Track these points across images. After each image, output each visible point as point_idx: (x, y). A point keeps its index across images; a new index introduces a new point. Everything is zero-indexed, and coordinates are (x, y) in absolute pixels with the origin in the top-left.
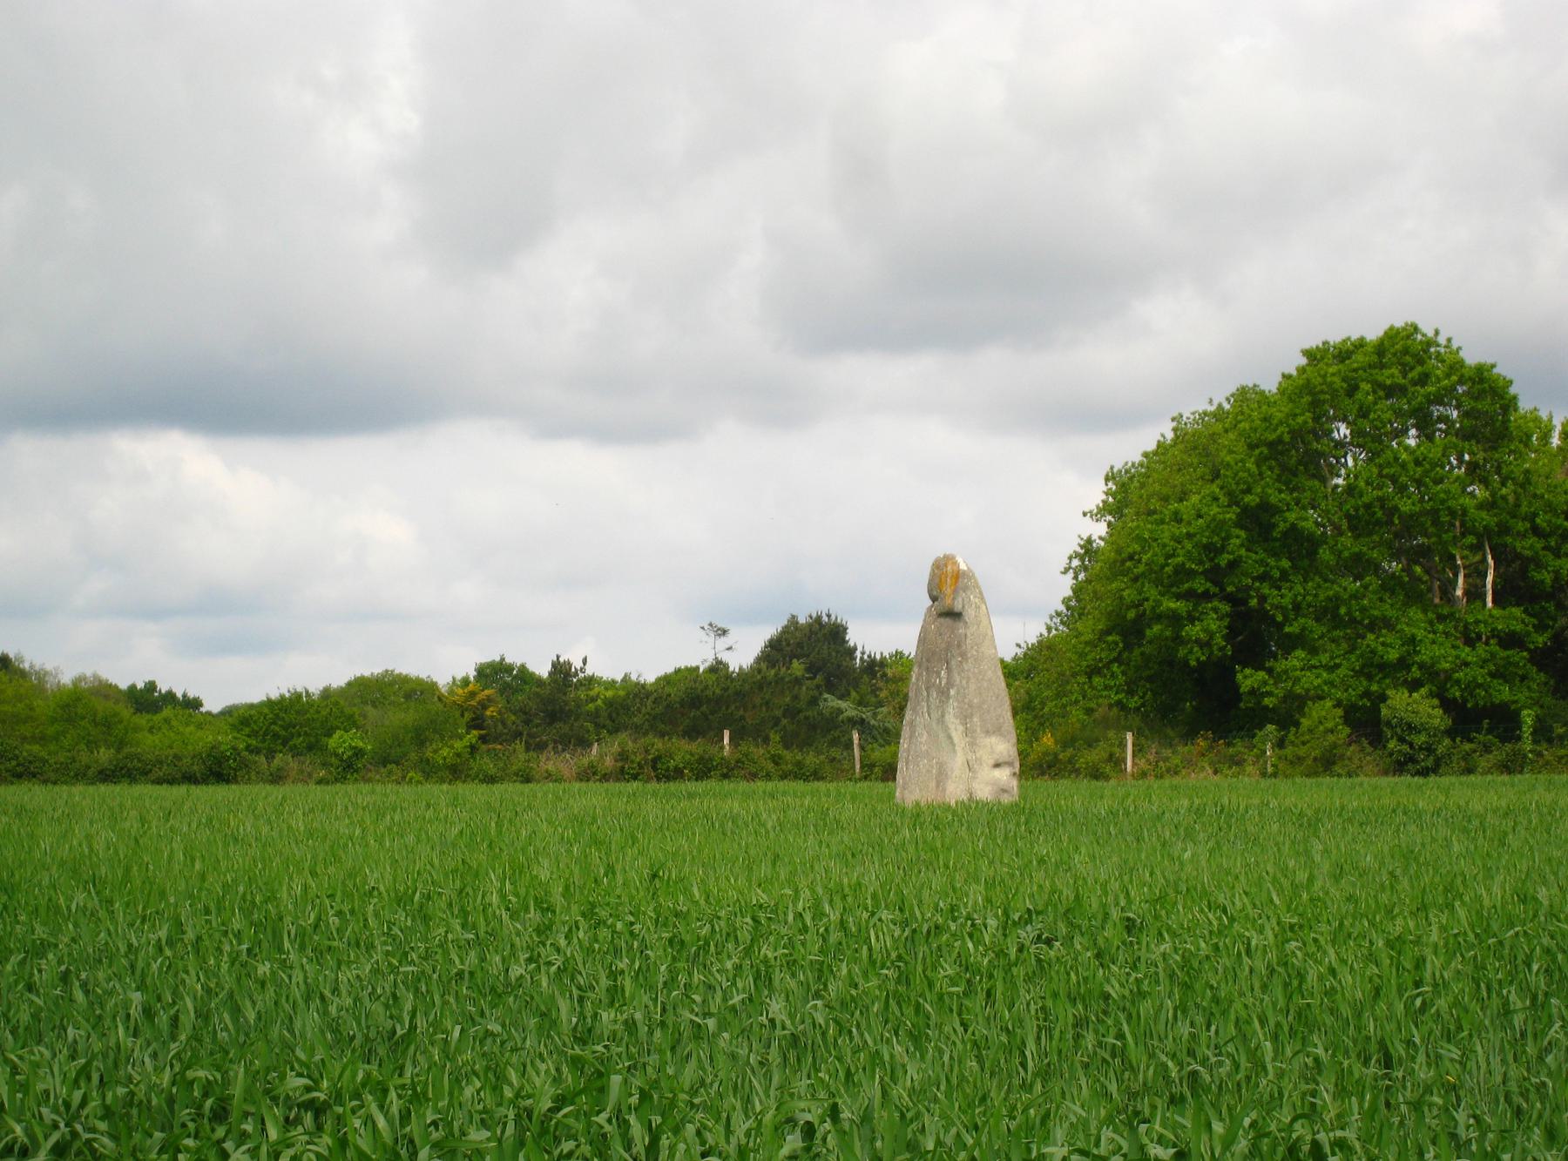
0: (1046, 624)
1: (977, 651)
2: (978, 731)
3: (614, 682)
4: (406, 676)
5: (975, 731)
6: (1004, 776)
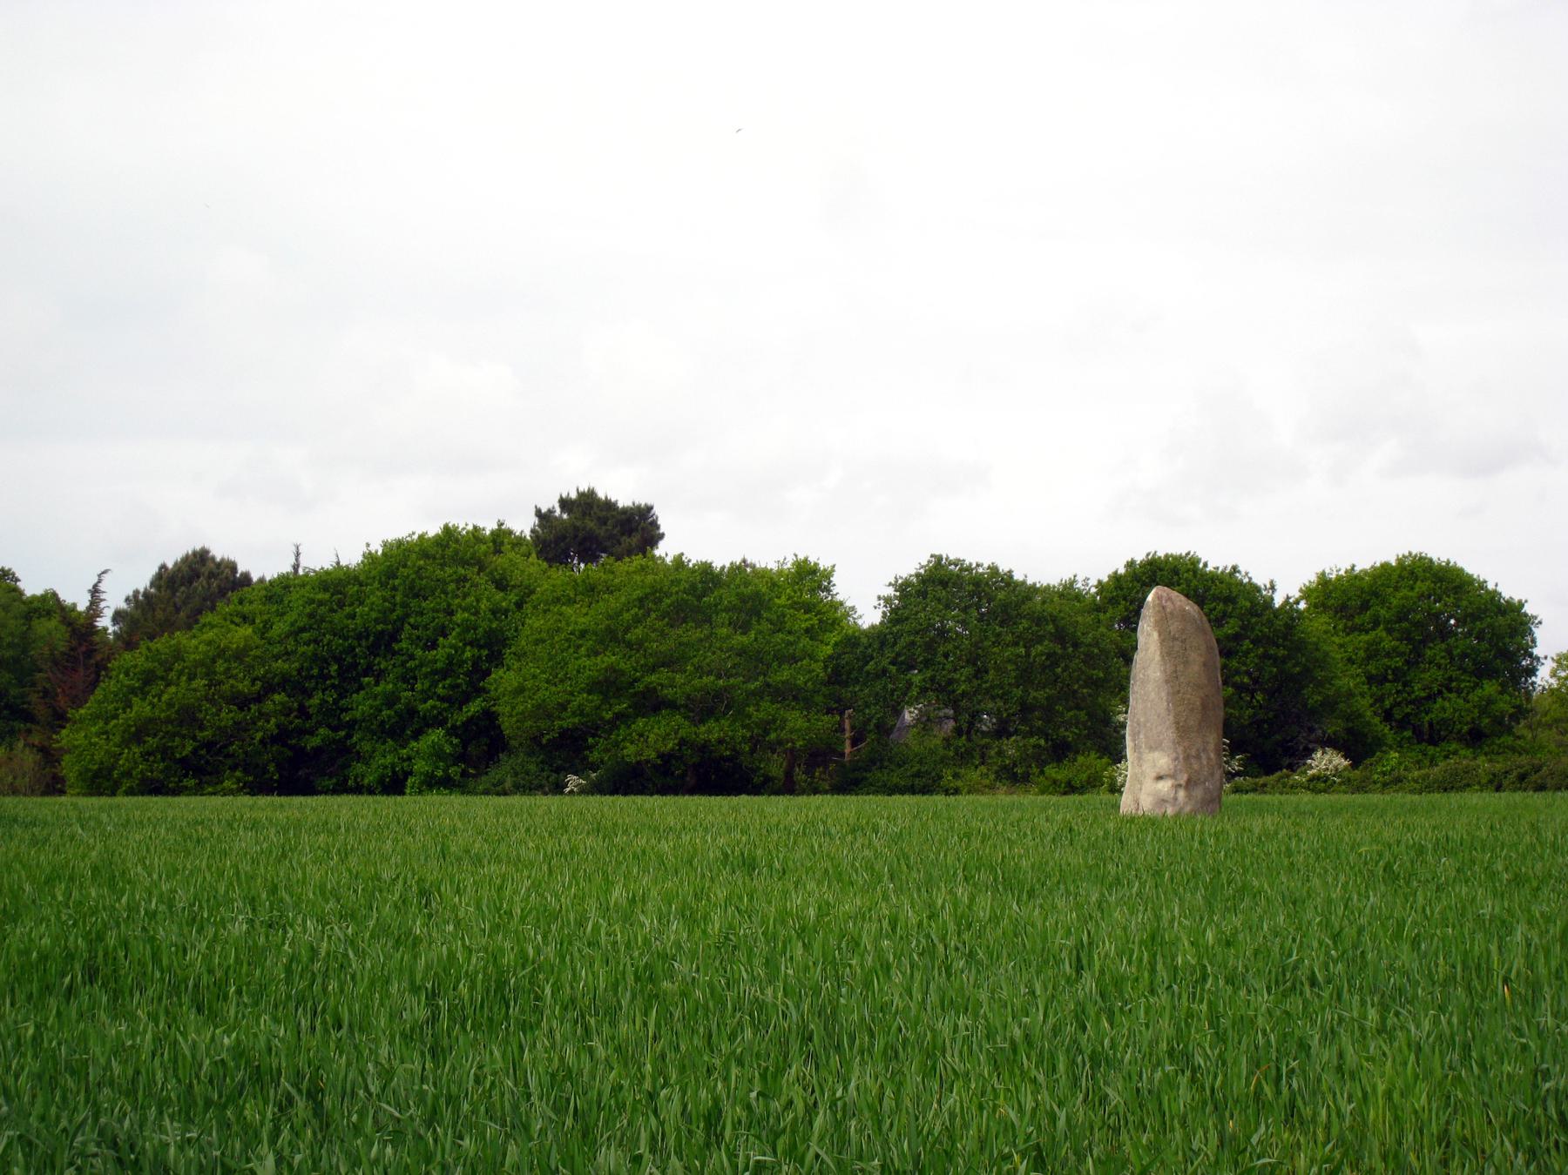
3: (501, 537)
4: (1400, 561)
5: (1141, 747)
6: (1165, 786)
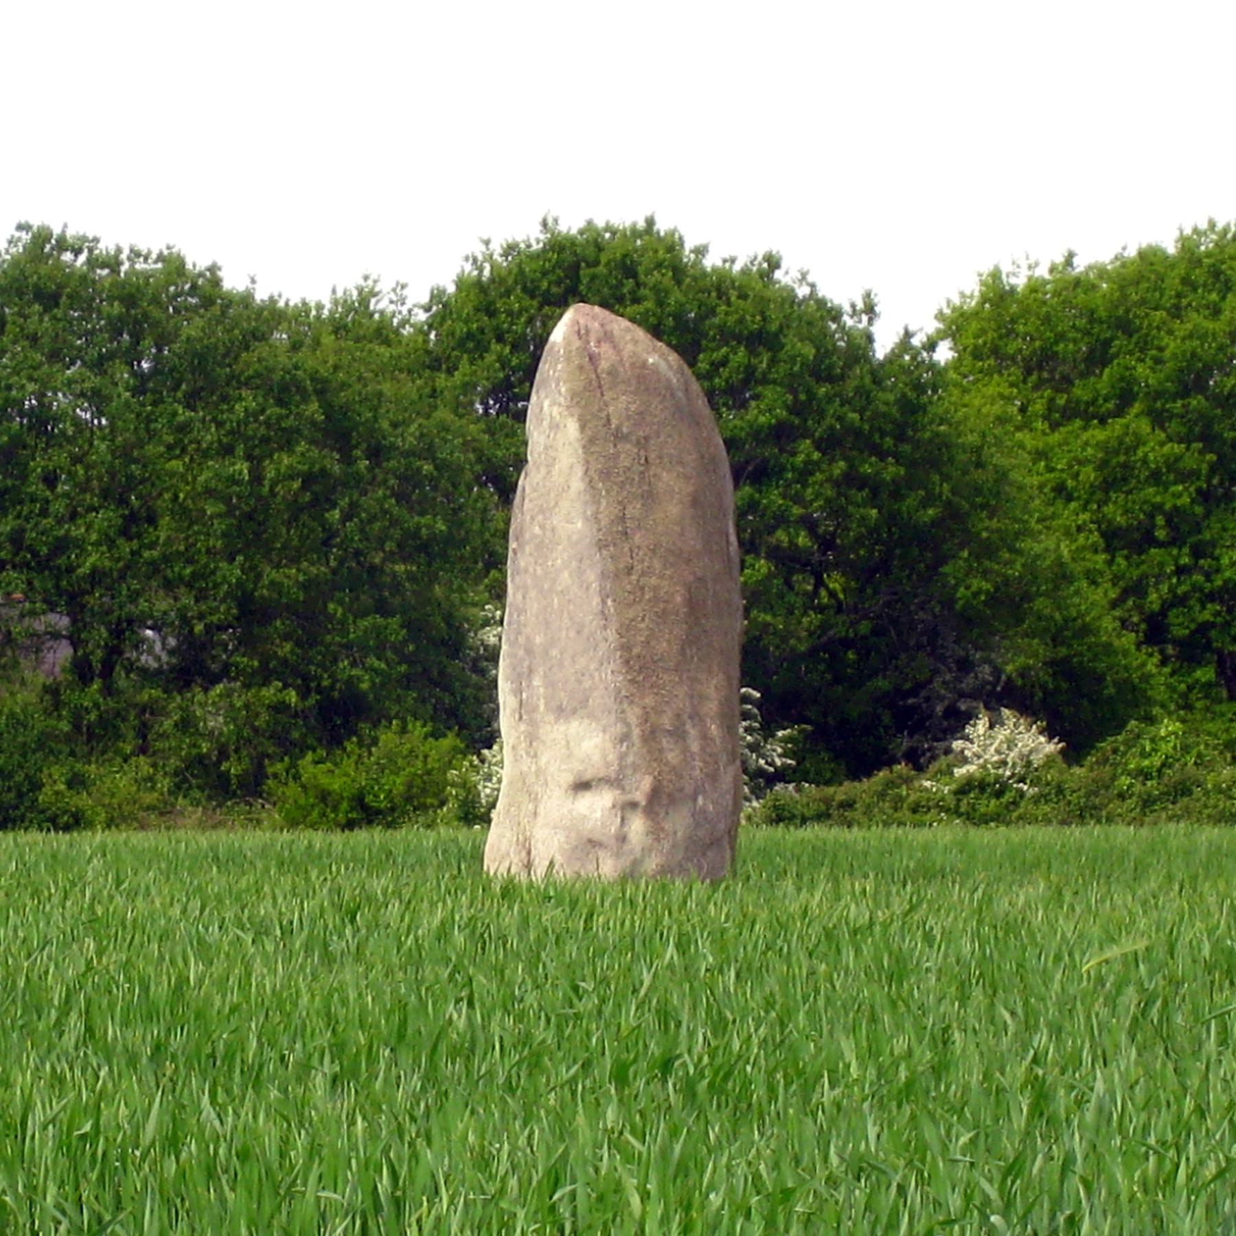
0: (1228, 225)
1: (542, 527)
2: (542, 708)
5: (535, 709)
